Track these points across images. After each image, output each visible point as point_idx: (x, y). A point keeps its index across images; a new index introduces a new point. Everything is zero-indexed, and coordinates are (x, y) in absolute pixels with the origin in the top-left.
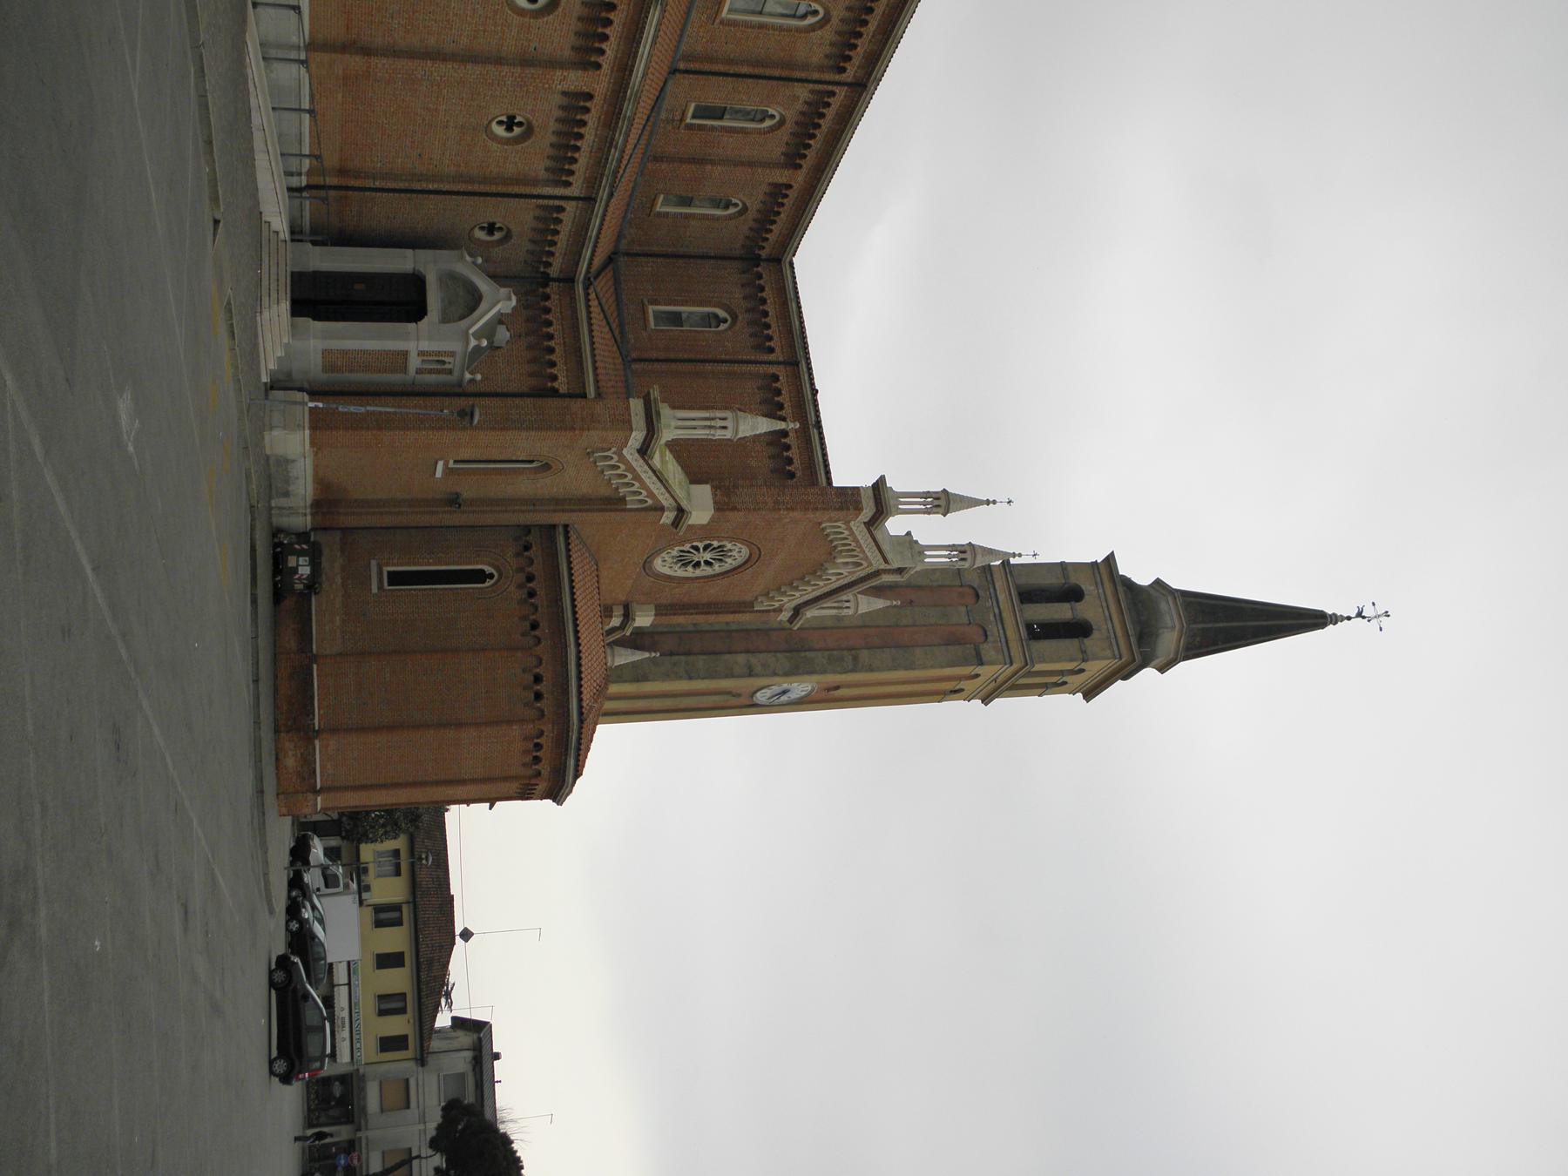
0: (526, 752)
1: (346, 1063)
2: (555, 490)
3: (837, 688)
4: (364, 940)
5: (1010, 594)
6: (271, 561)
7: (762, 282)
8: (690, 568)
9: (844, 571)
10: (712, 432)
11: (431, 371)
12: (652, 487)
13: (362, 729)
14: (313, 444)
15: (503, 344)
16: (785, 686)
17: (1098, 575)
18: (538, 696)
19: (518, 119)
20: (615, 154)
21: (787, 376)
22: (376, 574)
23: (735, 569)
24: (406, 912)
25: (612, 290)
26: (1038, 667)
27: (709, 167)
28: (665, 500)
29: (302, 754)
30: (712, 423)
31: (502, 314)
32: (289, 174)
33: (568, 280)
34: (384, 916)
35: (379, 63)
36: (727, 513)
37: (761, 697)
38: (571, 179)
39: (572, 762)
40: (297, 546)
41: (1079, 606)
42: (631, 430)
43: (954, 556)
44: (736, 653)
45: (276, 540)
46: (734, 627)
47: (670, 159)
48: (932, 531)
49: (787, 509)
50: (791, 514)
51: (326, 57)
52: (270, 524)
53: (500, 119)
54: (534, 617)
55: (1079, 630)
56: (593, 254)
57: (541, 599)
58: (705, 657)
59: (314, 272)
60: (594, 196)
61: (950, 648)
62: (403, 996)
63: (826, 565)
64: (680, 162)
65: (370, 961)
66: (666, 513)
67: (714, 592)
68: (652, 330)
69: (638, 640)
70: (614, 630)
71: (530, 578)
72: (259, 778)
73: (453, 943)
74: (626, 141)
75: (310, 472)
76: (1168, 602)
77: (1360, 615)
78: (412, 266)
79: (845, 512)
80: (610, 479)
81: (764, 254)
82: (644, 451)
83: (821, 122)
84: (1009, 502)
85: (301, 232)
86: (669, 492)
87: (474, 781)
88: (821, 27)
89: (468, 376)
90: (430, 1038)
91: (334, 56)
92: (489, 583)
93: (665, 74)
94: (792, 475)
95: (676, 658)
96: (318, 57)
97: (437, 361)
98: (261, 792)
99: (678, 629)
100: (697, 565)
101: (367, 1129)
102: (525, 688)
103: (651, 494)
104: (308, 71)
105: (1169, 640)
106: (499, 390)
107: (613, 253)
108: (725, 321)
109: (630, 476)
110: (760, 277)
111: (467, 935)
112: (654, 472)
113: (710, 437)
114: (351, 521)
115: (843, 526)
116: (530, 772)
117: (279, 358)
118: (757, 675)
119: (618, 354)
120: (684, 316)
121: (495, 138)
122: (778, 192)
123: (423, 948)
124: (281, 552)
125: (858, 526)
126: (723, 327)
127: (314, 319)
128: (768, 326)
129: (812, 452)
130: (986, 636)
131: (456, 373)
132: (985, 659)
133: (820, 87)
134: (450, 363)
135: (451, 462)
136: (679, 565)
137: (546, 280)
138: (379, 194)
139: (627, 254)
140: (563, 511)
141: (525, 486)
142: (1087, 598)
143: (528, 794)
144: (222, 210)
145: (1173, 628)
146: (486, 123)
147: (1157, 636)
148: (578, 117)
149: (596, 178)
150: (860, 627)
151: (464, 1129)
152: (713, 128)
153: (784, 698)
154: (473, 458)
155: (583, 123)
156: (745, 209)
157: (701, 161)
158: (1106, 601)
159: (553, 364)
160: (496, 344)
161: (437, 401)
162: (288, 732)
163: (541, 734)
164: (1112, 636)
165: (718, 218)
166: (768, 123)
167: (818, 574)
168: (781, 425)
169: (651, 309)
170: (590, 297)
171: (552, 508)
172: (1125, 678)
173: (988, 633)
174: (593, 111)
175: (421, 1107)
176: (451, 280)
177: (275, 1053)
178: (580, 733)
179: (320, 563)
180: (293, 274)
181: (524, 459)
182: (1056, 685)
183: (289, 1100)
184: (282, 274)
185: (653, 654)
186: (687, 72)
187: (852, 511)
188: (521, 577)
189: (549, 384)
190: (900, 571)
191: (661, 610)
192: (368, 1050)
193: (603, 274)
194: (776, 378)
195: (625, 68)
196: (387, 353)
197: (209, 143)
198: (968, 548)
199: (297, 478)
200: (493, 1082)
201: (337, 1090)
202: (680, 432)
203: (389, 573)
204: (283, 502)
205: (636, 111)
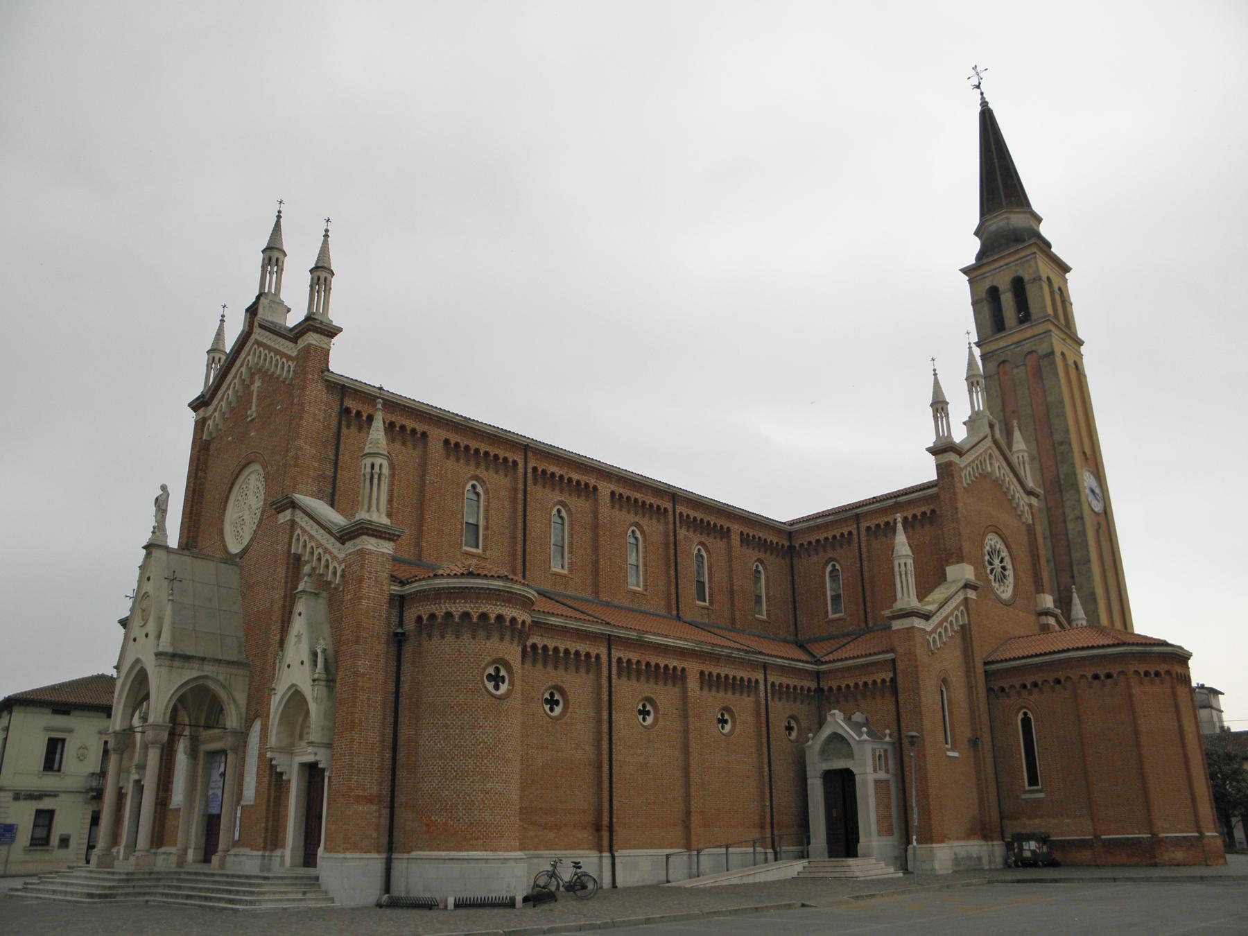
0: (1152, 682)
2: (960, 673)
3: (1084, 453)
6: (1028, 868)
7: (805, 543)
8: (1007, 573)
9: (996, 465)
10: (909, 572)
11: (887, 764)
12: (951, 608)
13: (1147, 803)
14: (942, 841)
15: (864, 716)
16: (1087, 491)
17: (977, 278)
18: (1109, 676)
20: (735, 654)
21: (866, 521)
23: (1004, 541)
25: (821, 644)
26: (1050, 311)
27: (735, 588)
28: (960, 597)
29: (1172, 847)
30: (903, 573)
31: (844, 718)
32: (766, 860)
33: (818, 675)
35: (695, 805)
36: (964, 554)
37: (1098, 507)
38: (753, 680)
39: (1156, 649)
40: (1016, 850)
41: (1001, 288)
42: (913, 627)
43: (976, 389)
45: (1013, 865)
46: (1048, 533)
47: (733, 613)
48: (961, 407)
49: (957, 512)
50: (960, 509)
51: (694, 838)
54: (1051, 682)
55: (1018, 286)
56: (800, 661)
57: (1039, 678)
58: (1072, 551)
59: (828, 843)
60: (763, 664)
63: (994, 478)
64: (734, 606)
66: (969, 596)
67: (1023, 553)
68: (845, 614)
69: (1064, 603)
70: (1058, 621)
71: (1024, 686)
72: (1191, 879)
74: (727, 647)
75: (963, 843)
76: (990, 225)
77: (978, 87)
78: (818, 779)
79: (954, 473)
80: (949, 637)
81: (787, 544)
82: (927, 617)
83: (699, 519)
85: (802, 852)
86: (954, 596)
87: (1179, 719)
88: (642, 527)
89: (887, 739)
91: (693, 833)
92: (1030, 715)
93: (681, 623)
94: (933, 511)
95: (1075, 572)
96: (694, 844)
97: (879, 760)
98: (1202, 878)
99: (1054, 574)
100: (1004, 568)
102: (1104, 686)
103: (956, 608)
104: (703, 849)
105: (1017, 220)
106: (895, 717)
107: (797, 645)
108: (834, 566)
109: (945, 624)
110: (802, 545)
112: (940, 608)
113: (913, 573)
114: (995, 817)
115: (964, 471)
117: (886, 865)
118: (1082, 513)
119: (864, 637)
120: (834, 593)
122: (745, 540)
124: (1021, 861)
125: (962, 462)
126: (838, 567)
127: (857, 841)
128: (834, 537)
129: (915, 499)
130: (1032, 352)
131: (886, 747)
133: (678, 523)
134: (880, 751)
135: (947, 746)
136: (1005, 580)
137: (819, 690)
138: (774, 803)
139: (797, 634)
140: (974, 667)
141: (959, 694)
143: (1185, 678)
144: (795, 902)
145: (1008, 218)
146: (724, 737)
148: (715, 679)
149: (751, 664)
150: (1037, 442)
152: (710, 588)
153: (1097, 490)
154: (942, 728)
155: (718, 675)
156: (759, 560)
157: (732, 593)
159: (875, 682)
160: (865, 721)
161: (906, 759)
162: (1155, 857)
163: (1137, 672)
165: (767, 577)
166: (703, 553)
167: (1000, 482)
168: (900, 526)
169: (831, 616)
170: (828, 660)
171: (972, 675)
172: (1049, 245)
173: (1030, 350)
174: (710, 670)
176: (824, 753)
178: (1133, 644)
179: (1026, 834)
180: (830, 856)
181: (940, 697)
184: (831, 864)
185: (1074, 590)
187: (953, 468)
188: (1024, 692)
189: (888, 684)
190: (991, 426)
191: (1040, 589)
193: (811, 651)
194: (868, 528)
195: (682, 653)
196: (876, 793)
197: (756, 909)
198: (970, 381)
199: (967, 851)
202: (911, 594)
204: (985, 861)
205: (708, 641)
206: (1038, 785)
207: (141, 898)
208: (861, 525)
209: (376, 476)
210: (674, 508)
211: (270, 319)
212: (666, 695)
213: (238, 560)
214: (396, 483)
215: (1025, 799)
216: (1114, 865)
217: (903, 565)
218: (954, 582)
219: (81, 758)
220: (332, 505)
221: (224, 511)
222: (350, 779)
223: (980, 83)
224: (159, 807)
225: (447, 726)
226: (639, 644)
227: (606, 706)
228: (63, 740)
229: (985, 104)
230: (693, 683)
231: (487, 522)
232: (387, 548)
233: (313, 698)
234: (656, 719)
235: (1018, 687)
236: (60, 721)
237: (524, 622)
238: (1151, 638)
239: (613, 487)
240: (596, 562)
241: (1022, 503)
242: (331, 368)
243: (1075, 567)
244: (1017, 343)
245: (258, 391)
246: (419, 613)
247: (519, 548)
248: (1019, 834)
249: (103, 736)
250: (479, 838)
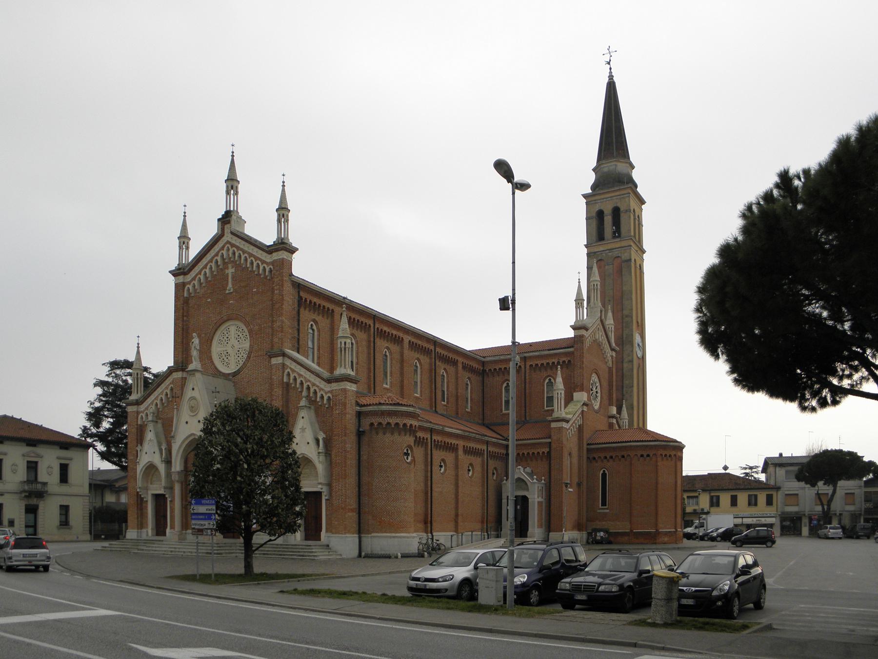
0: (667, 459)
1: (776, 520)
5: (600, 245)
8: (598, 395)
9: (601, 334)
18: (648, 456)
19: (405, 451)
26: (632, 234)
30: (559, 398)
34: (715, 503)
35: (460, 512)
37: (640, 355)
39: (672, 444)
40: (593, 536)
41: (606, 212)
44: (623, 367)
47: (457, 409)
52: (585, 545)
53: (406, 458)
55: (616, 212)
61: (623, 273)
62: (750, 496)
65: (734, 509)
67: (605, 384)
69: (619, 411)
71: (606, 458)
73: (729, 474)
76: (604, 167)
81: (482, 369)
84: (579, 273)
89: (543, 481)
90: (769, 485)
92: (606, 472)
94: (569, 361)
98: (678, 548)
100: (597, 392)
101: (805, 511)
102: (645, 460)
103: (578, 416)
105: (621, 167)
111: (726, 468)
116: (674, 458)
118: (633, 358)
120: (506, 399)
122: (412, 346)
123: (730, 487)
130: (619, 257)
132: (628, 258)
142: (602, 208)
145: (616, 165)
151: (808, 473)
152: (448, 394)
153: (641, 344)
158: (603, 199)
163: (661, 455)
164: (619, 197)
165: (471, 388)
169: (504, 412)
172: (636, 186)
173: (617, 256)
175: (798, 489)
177: (765, 546)
178: (662, 441)
182: (639, 221)
186: (435, 407)
188: (605, 461)
191: (611, 404)
192: (771, 510)
194: (531, 366)
195: (457, 436)
200: (792, 457)
201: (788, 523)
203: (602, 506)
206: (606, 506)
207: (233, 555)
208: (527, 363)
210: (435, 349)
211: (237, 229)
212: (449, 457)
214: (321, 339)
215: (599, 513)
217: (559, 394)
218: (578, 401)
219: (14, 472)
220: (298, 352)
222: (345, 501)
223: (610, 60)
224: (184, 510)
225: (388, 477)
226: (442, 433)
227: (429, 463)
229: (612, 77)
230: (461, 452)
231: (358, 360)
232: (352, 387)
233: (319, 461)
234: (445, 470)
235: (602, 458)
237: (415, 426)
238: (669, 438)
239: (410, 338)
240: (402, 381)
241: (609, 355)
243: (624, 389)
245: (232, 275)
246: (372, 421)
248: (595, 529)
249: (26, 458)
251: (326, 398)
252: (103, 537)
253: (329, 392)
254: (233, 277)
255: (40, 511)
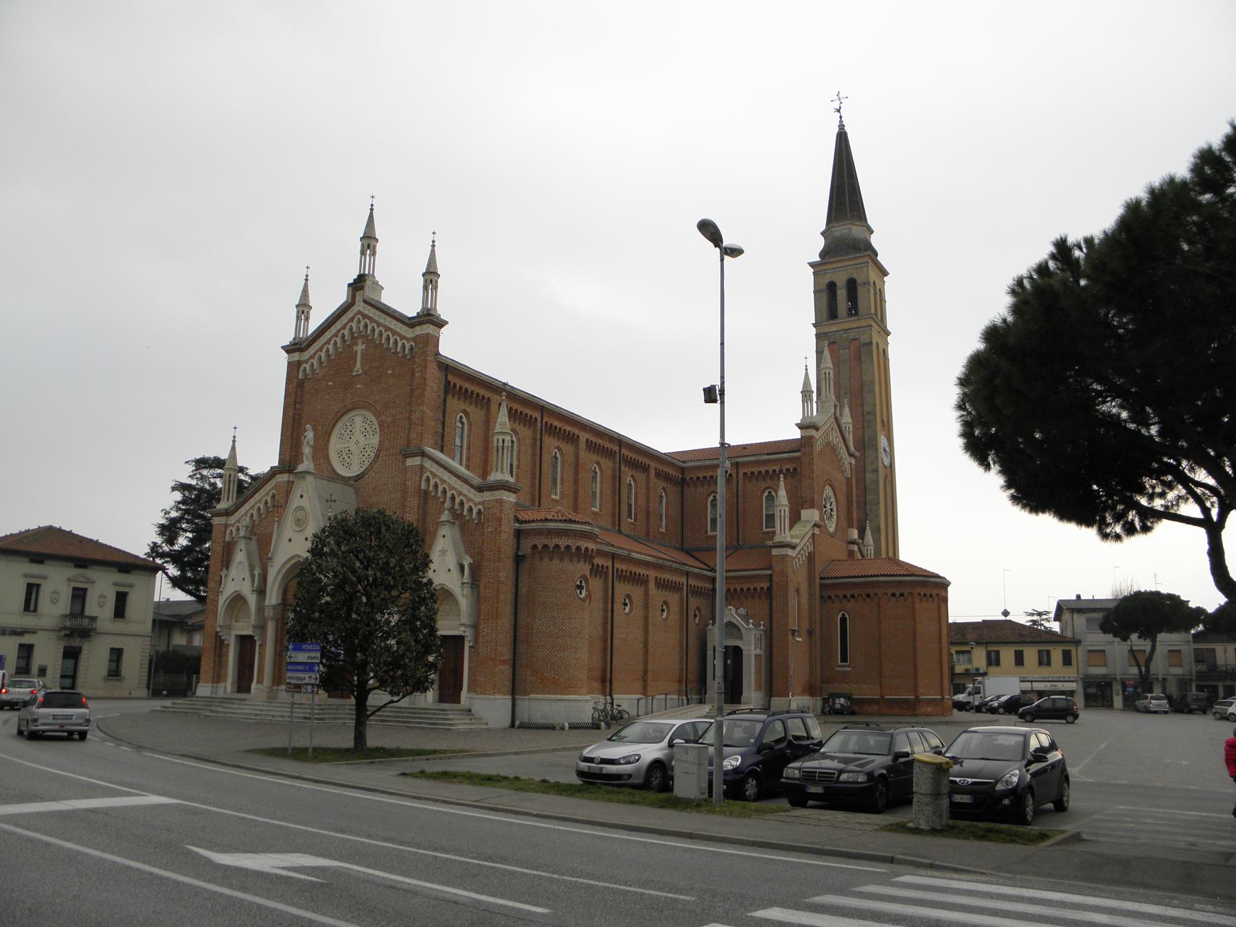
0: (927, 601)
3: (883, 421)
4: (1008, 673)
9: (835, 435)
13: (916, 675)
16: (882, 450)
18: (902, 595)
19: (578, 583)
22: (841, 667)
24: (992, 648)
26: (873, 311)
34: (994, 660)
35: (650, 667)
39: (932, 579)
47: (648, 528)
55: (852, 285)
57: (855, 592)
62: (1039, 651)
65: (1019, 669)
67: (842, 499)
69: (862, 534)
71: (845, 596)
73: (1010, 621)
77: (839, 111)
81: (681, 476)
84: (235, 428)
89: (762, 627)
92: (847, 616)
94: (795, 469)
100: (832, 510)
101: (1115, 675)
103: (808, 541)
105: (856, 231)
111: (1006, 613)
114: (819, 679)
116: (936, 599)
121: (667, 617)
122: (591, 446)
123: (1013, 640)
127: (742, 694)
130: (856, 339)
145: (850, 229)
147: (855, 239)
151: (1116, 621)
152: (635, 509)
153: (887, 449)
163: (919, 594)
165: (667, 501)
166: (632, 483)
169: (709, 533)
172: (876, 254)
177: (1064, 721)
182: (881, 295)
183: (1089, 718)
188: (844, 601)
191: (850, 526)
192: (1070, 672)
194: (745, 474)
195: (647, 565)
200: (1093, 601)
201: (1093, 690)
208: (740, 471)
209: (500, 448)
211: (372, 297)
212: (637, 592)
213: (352, 482)
216: (891, 715)
217: (783, 511)
218: (806, 522)
219: (54, 601)
220: (442, 451)
221: (328, 441)
224: (277, 657)
225: (554, 617)
226: (628, 560)
227: (609, 600)
228: (38, 586)
230: (652, 585)
232: (510, 498)
233: (463, 595)
234: (631, 609)
236: (36, 569)
242: (441, 352)
243: (868, 507)
244: (846, 330)
247: (537, 481)
250: (573, 687)
251: (475, 511)
252: (165, 693)
253: (479, 503)
254: (363, 355)
255: (84, 656)
